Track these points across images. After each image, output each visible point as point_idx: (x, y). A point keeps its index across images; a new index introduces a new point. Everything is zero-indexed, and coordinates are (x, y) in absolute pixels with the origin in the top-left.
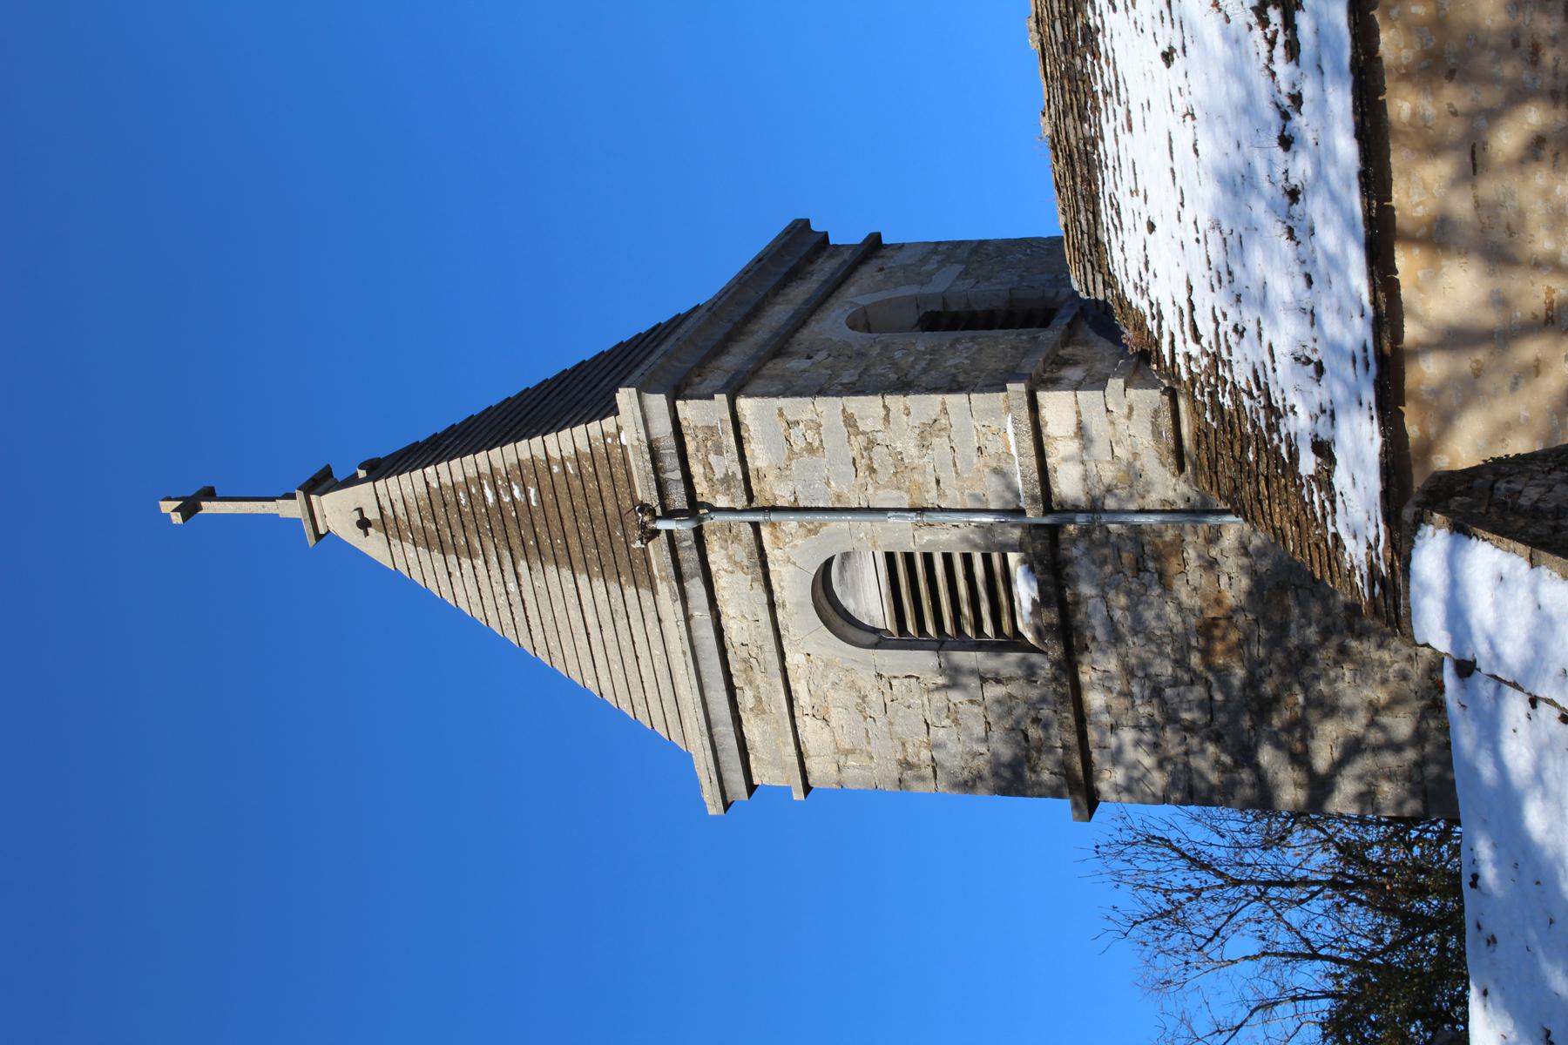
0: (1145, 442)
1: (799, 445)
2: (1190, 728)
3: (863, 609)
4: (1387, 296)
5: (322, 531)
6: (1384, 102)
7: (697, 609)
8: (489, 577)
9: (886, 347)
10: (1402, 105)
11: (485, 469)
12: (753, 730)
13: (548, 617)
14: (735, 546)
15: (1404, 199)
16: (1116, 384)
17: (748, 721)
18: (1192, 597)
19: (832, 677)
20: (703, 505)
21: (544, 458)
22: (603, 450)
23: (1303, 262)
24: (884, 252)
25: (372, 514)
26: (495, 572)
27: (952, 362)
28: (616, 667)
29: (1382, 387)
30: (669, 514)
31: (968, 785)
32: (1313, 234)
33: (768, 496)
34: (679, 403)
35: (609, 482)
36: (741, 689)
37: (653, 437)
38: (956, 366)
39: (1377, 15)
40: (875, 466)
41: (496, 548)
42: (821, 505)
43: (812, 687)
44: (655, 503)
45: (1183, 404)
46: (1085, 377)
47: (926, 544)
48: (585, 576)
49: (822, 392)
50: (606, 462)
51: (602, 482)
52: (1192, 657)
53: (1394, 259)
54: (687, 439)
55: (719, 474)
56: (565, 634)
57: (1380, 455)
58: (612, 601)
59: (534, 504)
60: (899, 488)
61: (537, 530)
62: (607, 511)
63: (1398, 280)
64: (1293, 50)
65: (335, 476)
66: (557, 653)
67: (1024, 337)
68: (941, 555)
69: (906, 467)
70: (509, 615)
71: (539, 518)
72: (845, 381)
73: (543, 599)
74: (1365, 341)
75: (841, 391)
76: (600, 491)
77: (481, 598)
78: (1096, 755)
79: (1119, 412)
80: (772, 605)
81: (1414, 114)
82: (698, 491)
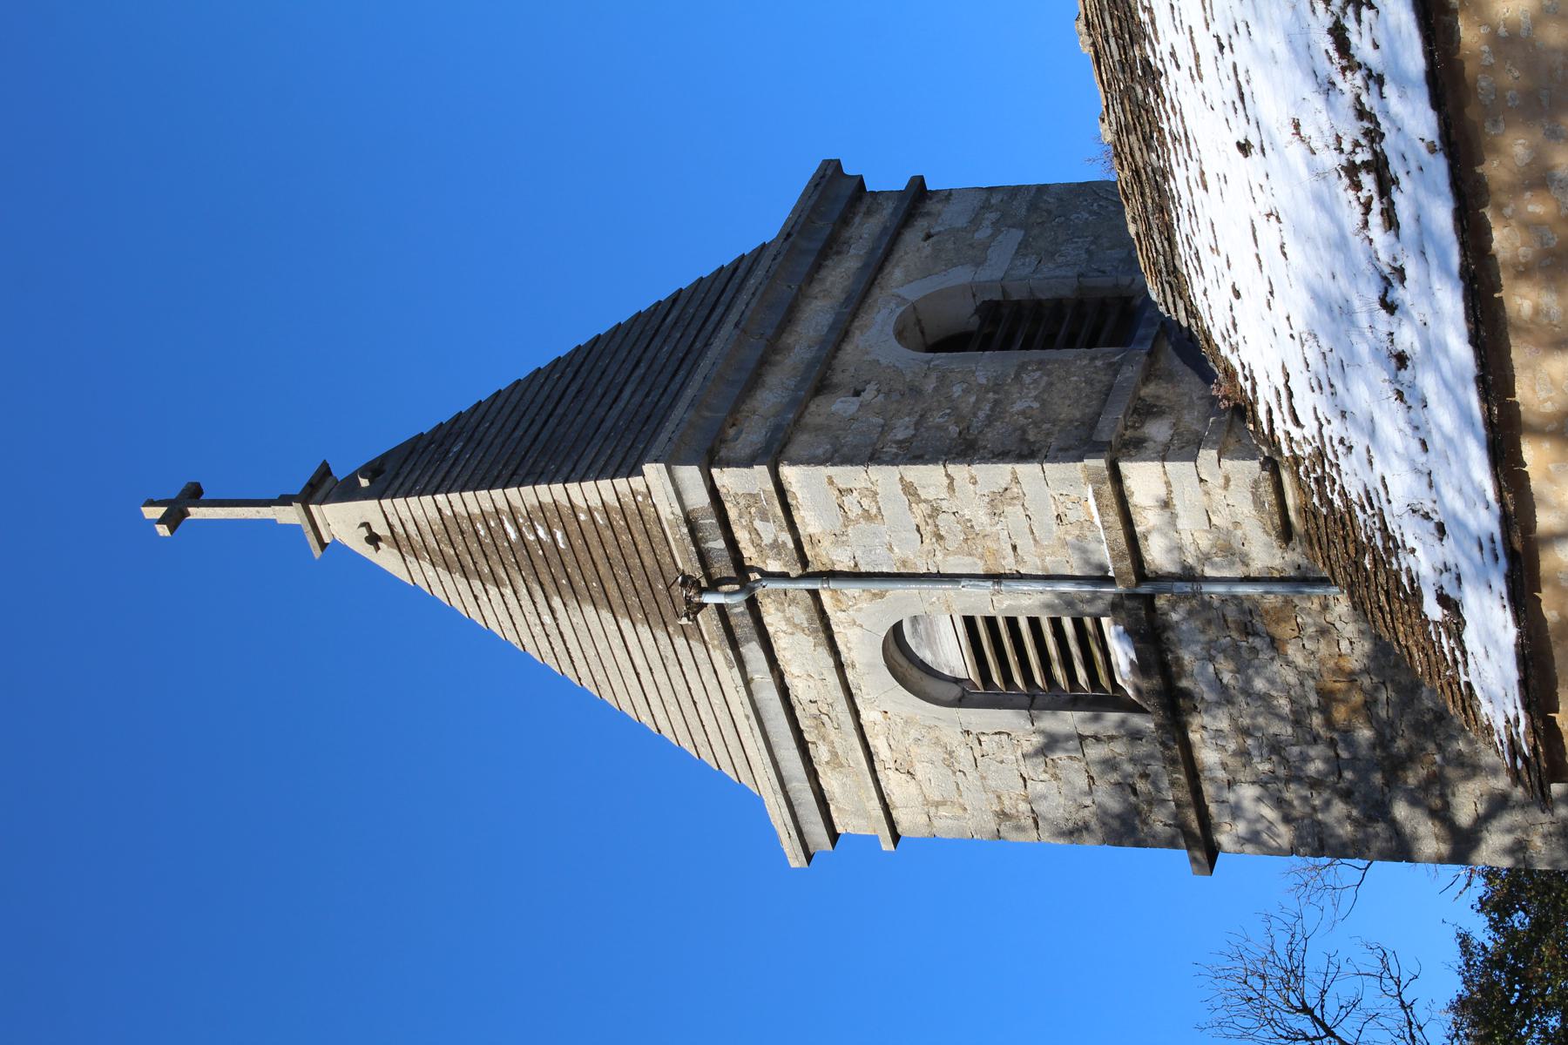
0: (1246, 511)
1: (855, 511)
2: (1315, 784)
3: (942, 660)
4: (1515, 497)
5: (327, 540)
6: (1500, 299)
7: (757, 672)
8: (521, 606)
9: (942, 379)
10: (1521, 300)
11: (502, 505)
12: (830, 782)
13: (591, 653)
14: (793, 608)
15: (1529, 395)
16: (1208, 455)
17: (825, 774)
18: (1309, 661)
19: (913, 733)
20: (753, 569)
21: (568, 505)
22: (634, 507)
23: (1417, 428)
24: (932, 206)
25: (381, 529)
26: (526, 601)
27: (1018, 406)
28: (673, 709)
29: (1513, 582)
30: (714, 585)
31: (1075, 832)
32: (1426, 406)
33: (825, 560)
34: (715, 471)
35: (644, 537)
36: (814, 743)
37: (689, 508)
38: (1023, 413)
39: (1489, 213)
40: (942, 533)
41: (524, 581)
42: (885, 570)
43: (892, 742)
44: (698, 574)
45: (1286, 477)
46: (1172, 436)
47: (1006, 609)
48: (627, 621)
49: (874, 457)
50: (638, 518)
51: (636, 535)
52: (1314, 718)
53: (1521, 452)
54: (728, 505)
55: (767, 539)
56: (613, 672)
57: (1516, 645)
58: (661, 648)
59: (562, 545)
60: (970, 555)
61: (569, 570)
62: (646, 564)
63: (1527, 472)
64: (1391, 222)
65: (334, 475)
66: (605, 687)
67: (1099, 363)
68: (1026, 620)
69: (977, 534)
70: (547, 644)
71: (569, 559)
72: (900, 437)
73: (583, 634)
74: (1492, 534)
75: (896, 455)
76: (635, 544)
77: (514, 625)
78: (1213, 808)
79: (1215, 482)
80: (840, 667)
81: (1537, 311)
82: (746, 554)
